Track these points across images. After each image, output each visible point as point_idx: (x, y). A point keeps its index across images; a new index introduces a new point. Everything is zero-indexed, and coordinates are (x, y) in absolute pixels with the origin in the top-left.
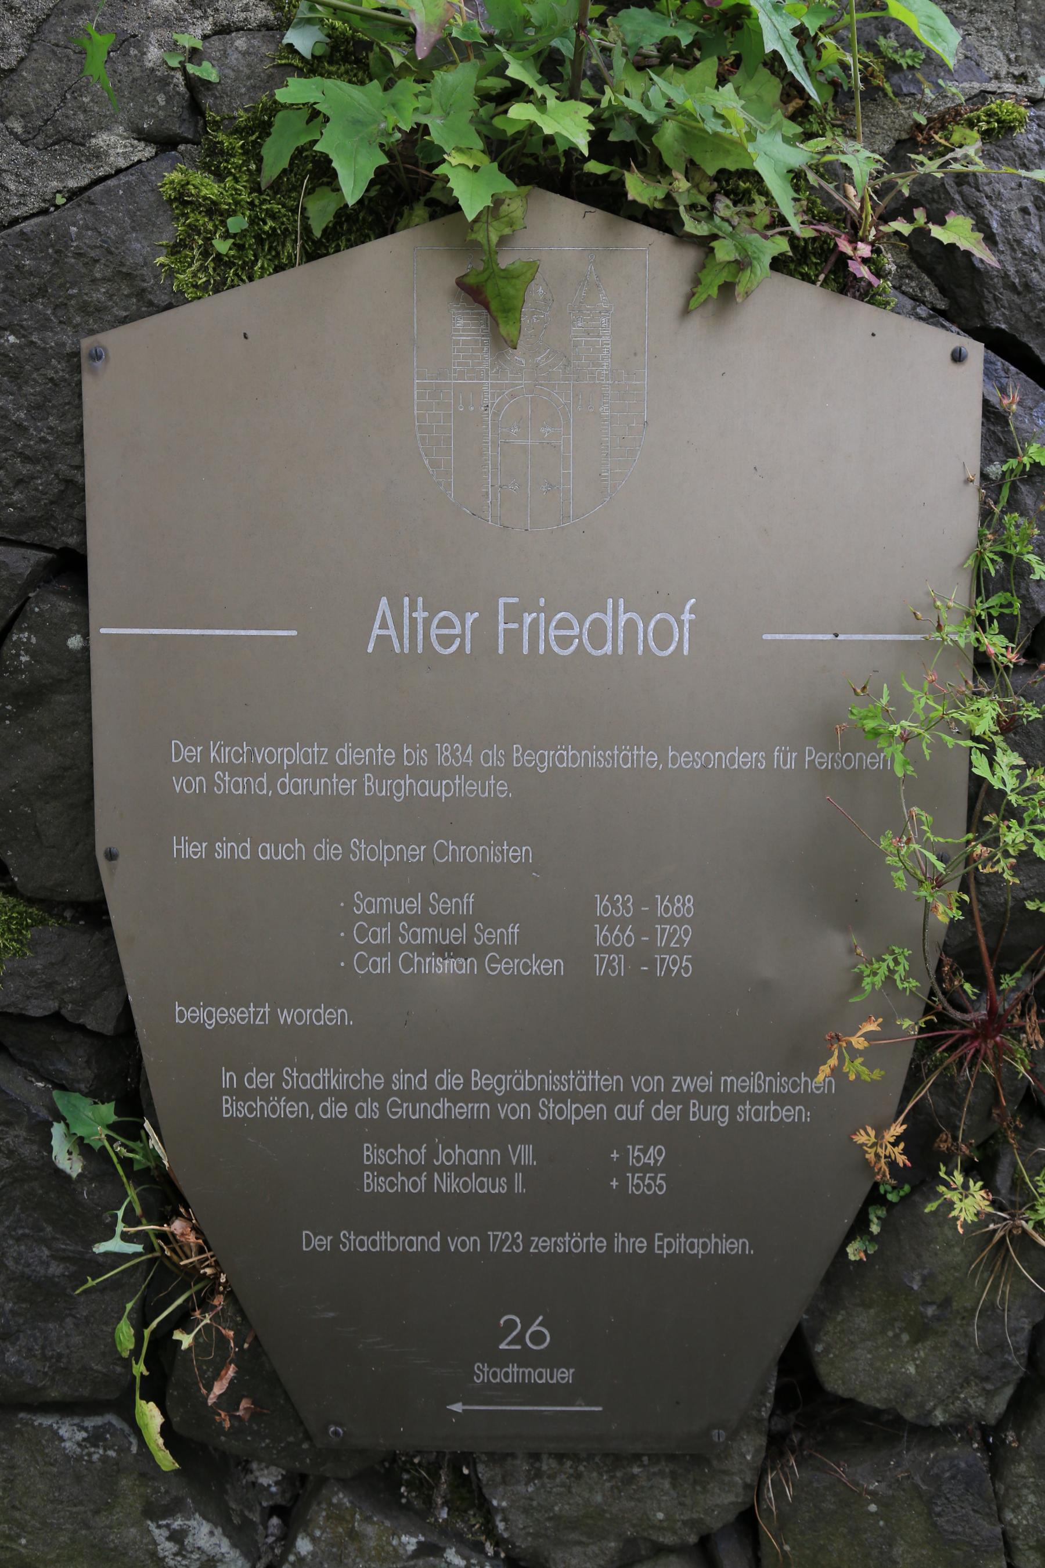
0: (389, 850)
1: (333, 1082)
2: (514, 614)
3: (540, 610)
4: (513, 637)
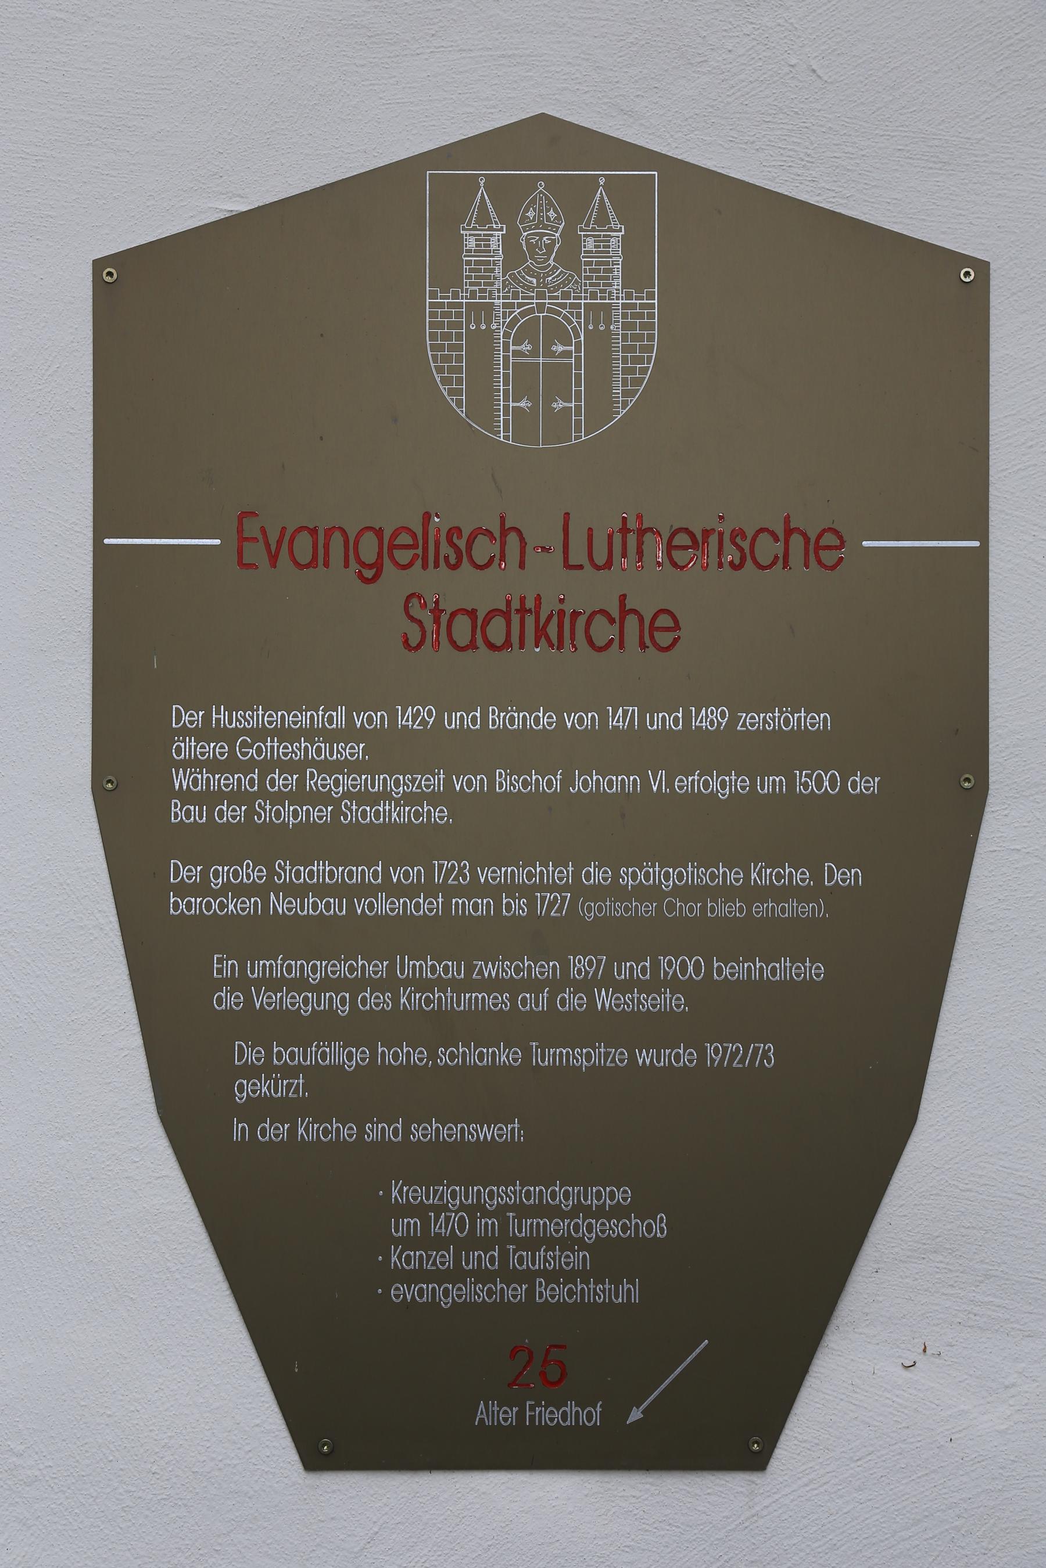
0: (295, 811)
1: (394, 815)
2: (532, 1408)
3: (542, 1406)
4: (532, 1418)
